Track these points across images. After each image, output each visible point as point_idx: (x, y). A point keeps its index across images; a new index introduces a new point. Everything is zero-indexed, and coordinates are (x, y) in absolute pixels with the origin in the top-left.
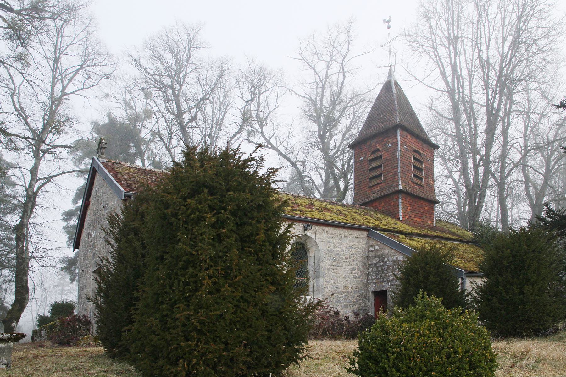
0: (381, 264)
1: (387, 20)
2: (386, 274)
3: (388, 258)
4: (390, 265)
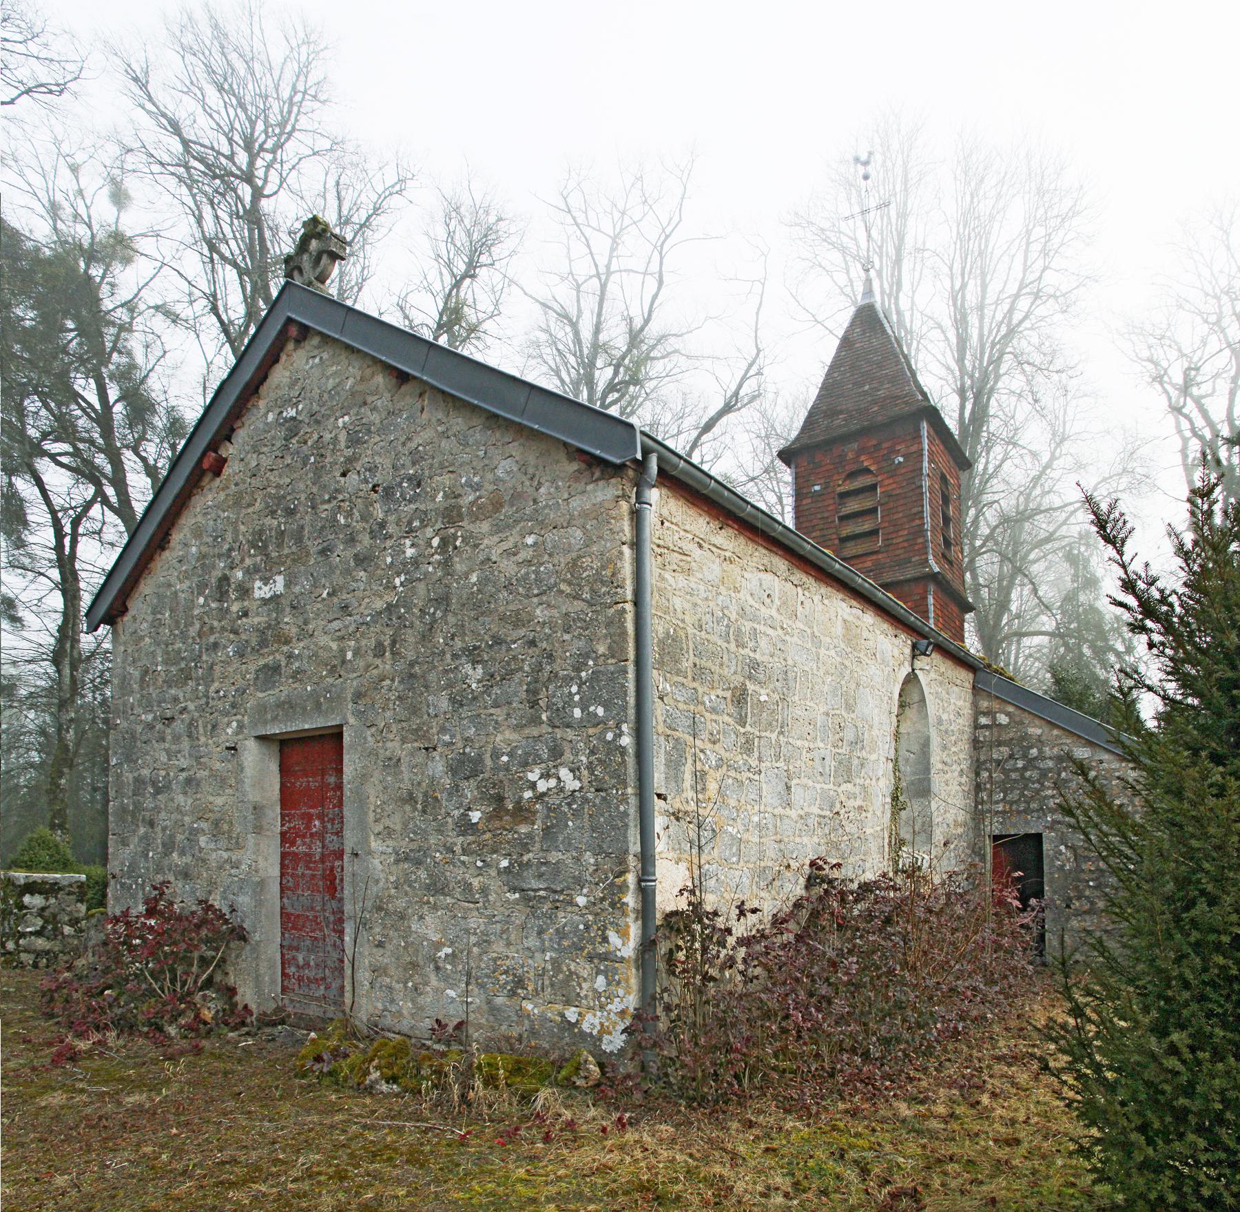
0: (1020, 764)
1: (864, 158)
2: (1038, 792)
3: (1040, 751)
4: (1050, 770)
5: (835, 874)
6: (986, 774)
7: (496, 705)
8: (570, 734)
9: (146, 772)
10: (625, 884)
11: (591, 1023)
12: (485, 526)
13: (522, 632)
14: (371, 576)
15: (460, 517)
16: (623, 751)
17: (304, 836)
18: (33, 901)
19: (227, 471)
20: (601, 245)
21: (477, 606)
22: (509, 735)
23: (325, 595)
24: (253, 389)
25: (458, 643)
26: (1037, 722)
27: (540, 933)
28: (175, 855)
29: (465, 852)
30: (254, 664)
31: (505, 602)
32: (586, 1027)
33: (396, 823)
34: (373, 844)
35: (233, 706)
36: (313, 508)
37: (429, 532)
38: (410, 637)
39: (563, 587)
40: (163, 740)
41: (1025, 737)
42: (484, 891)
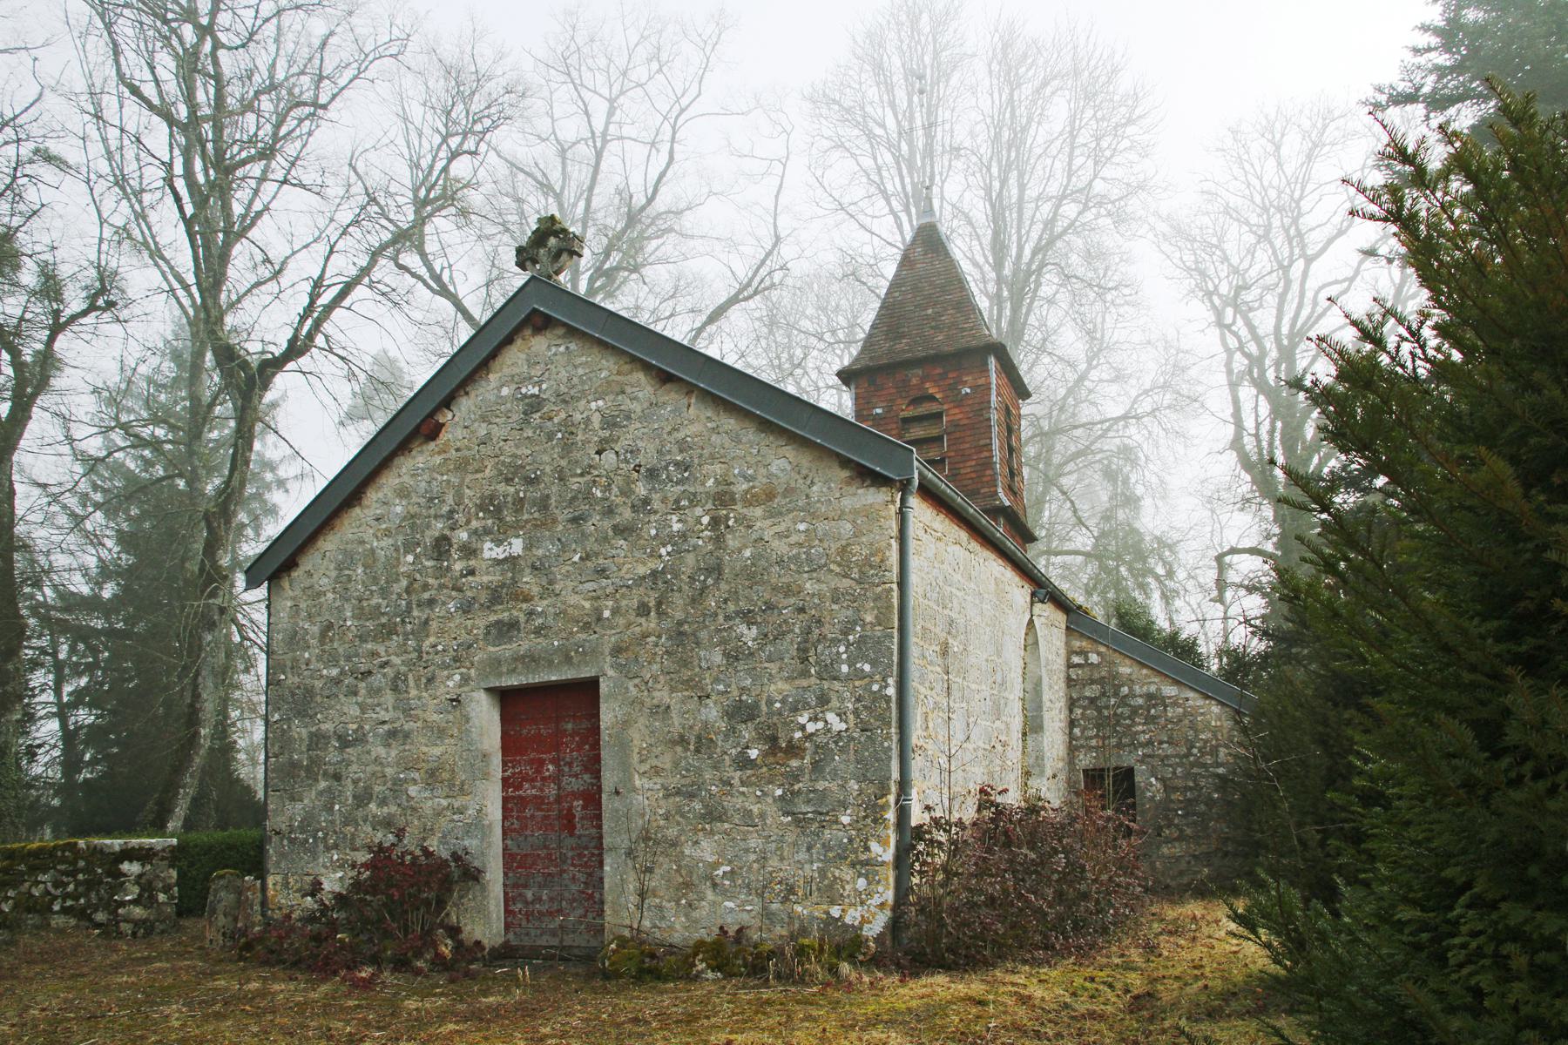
0: (1113, 701)
4: (1141, 707)
5: (999, 799)
6: (1079, 711)
7: (770, 660)
8: (837, 685)
9: (327, 727)
10: (887, 805)
11: (852, 916)
12: (758, 512)
13: (792, 601)
14: (633, 545)
15: (733, 501)
16: (888, 699)
17: (533, 780)
18: (131, 868)
19: (444, 436)
20: (599, 109)
21: (751, 577)
22: (781, 685)
23: (576, 558)
24: (485, 365)
25: (731, 607)
26: (1127, 661)
27: (809, 849)
28: (373, 806)
29: (743, 783)
30: (481, 621)
31: (776, 576)
32: (848, 920)
33: (666, 762)
34: (638, 783)
35: (456, 659)
36: (561, 479)
37: (698, 511)
38: (678, 600)
39: (832, 567)
40: (355, 694)
41: (1116, 676)
42: (762, 815)
